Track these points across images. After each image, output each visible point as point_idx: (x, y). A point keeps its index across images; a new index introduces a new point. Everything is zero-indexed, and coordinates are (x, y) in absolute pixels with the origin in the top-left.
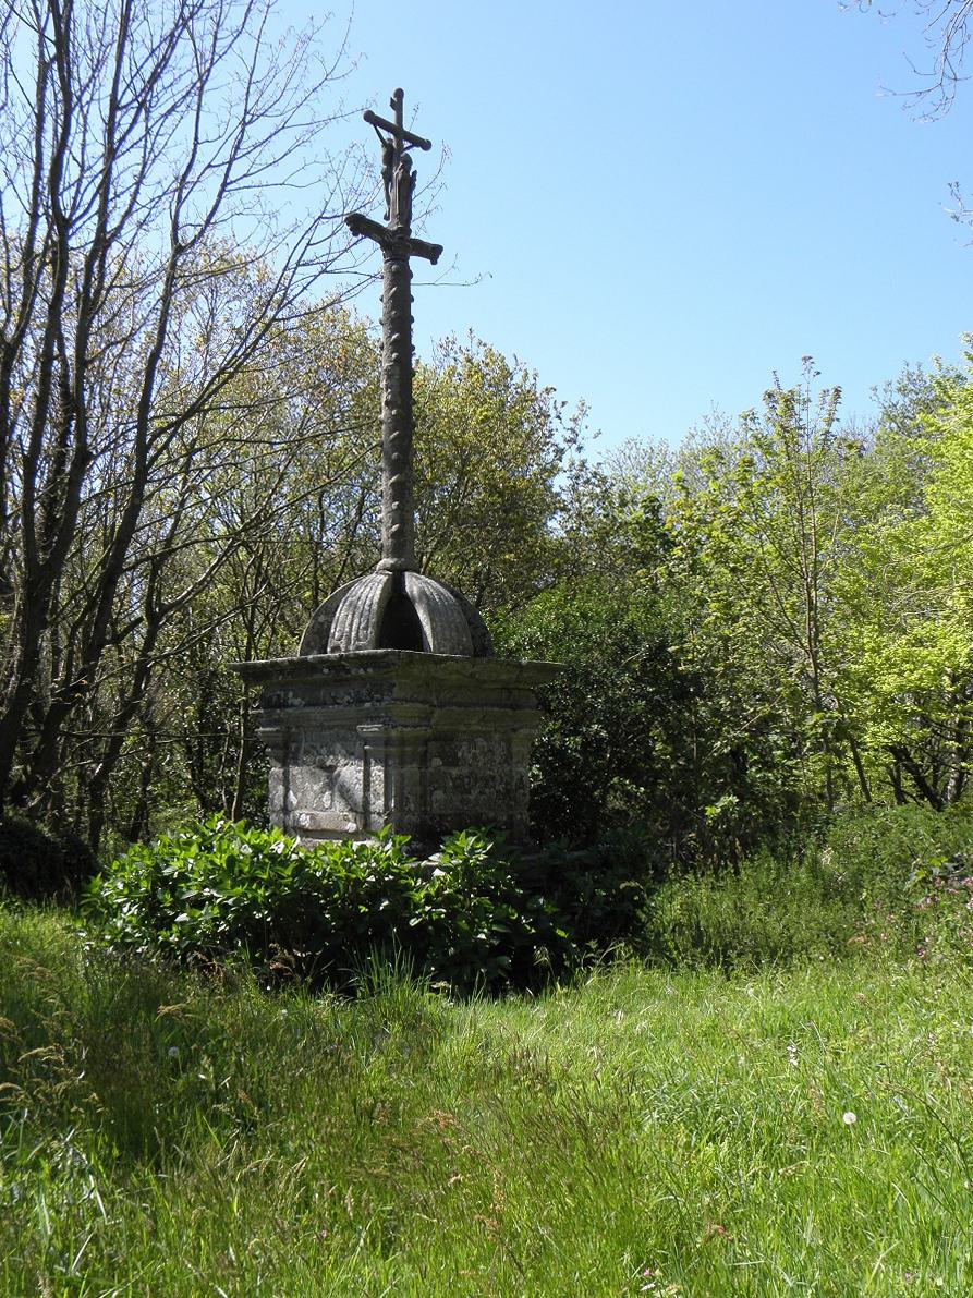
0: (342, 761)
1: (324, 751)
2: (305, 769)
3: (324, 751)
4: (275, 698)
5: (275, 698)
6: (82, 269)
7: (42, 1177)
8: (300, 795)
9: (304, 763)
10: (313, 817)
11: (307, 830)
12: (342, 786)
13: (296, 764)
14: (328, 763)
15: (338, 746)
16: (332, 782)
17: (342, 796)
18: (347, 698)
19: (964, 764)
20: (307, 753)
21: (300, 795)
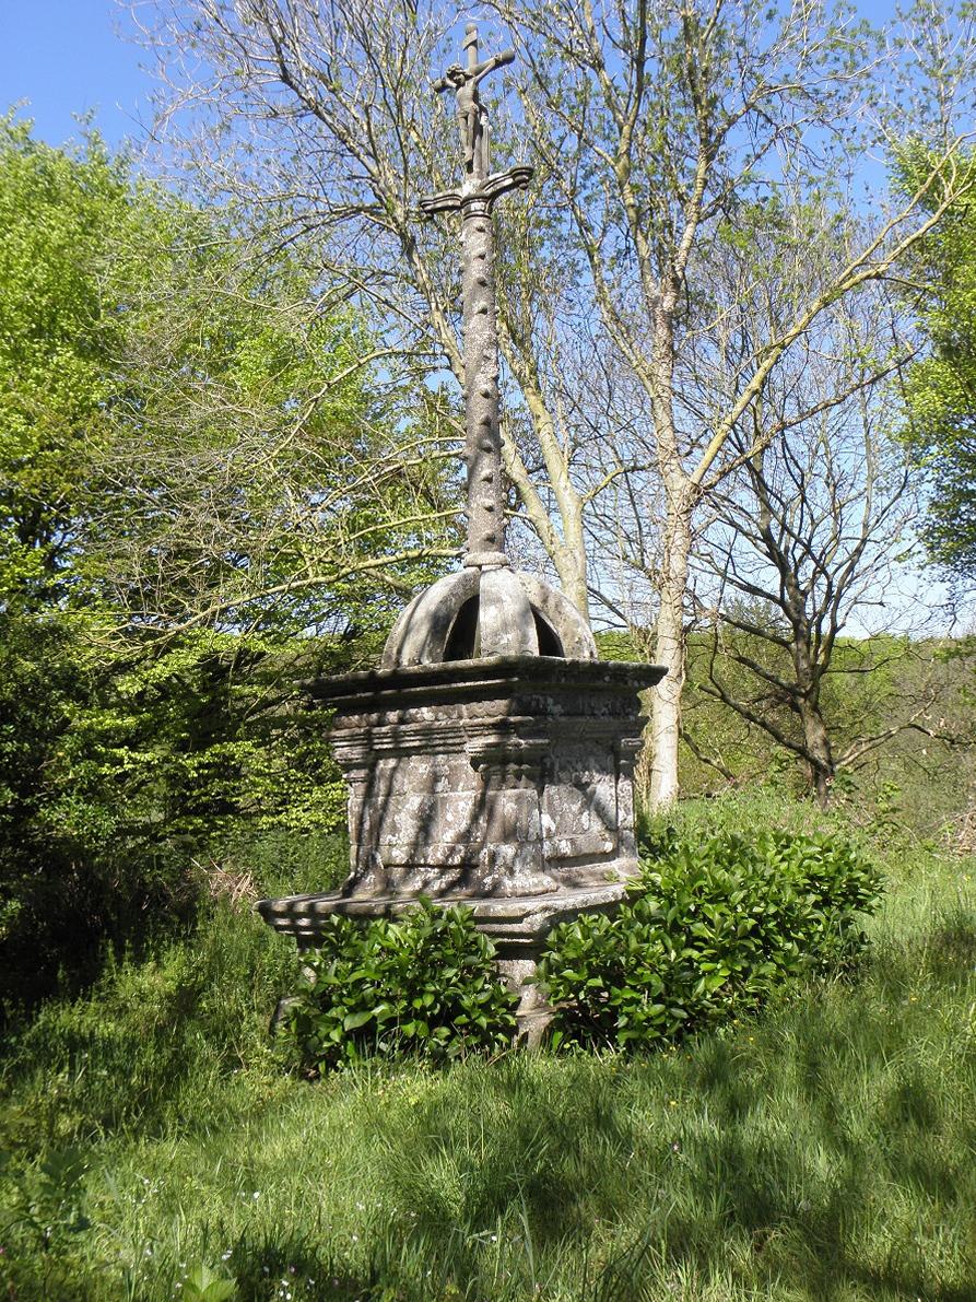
0: (597, 777)
1: (579, 766)
2: (563, 788)
3: (579, 766)
4: (534, 704)
5: (534, 704)
6: (970, 251)
7: (265, 1156)
8: (558, 818)
9: (560, 781)
10: (573, 841)
11: (569, 858)
12: (598, 804)
13: (552, 782)
14: (584, 780)
15: (592, 760)
16: (591, 802)
17: (599, 815)
18: (604, 709)
19: (277, 183)
20: (563, 769)
21: (558, 818)
